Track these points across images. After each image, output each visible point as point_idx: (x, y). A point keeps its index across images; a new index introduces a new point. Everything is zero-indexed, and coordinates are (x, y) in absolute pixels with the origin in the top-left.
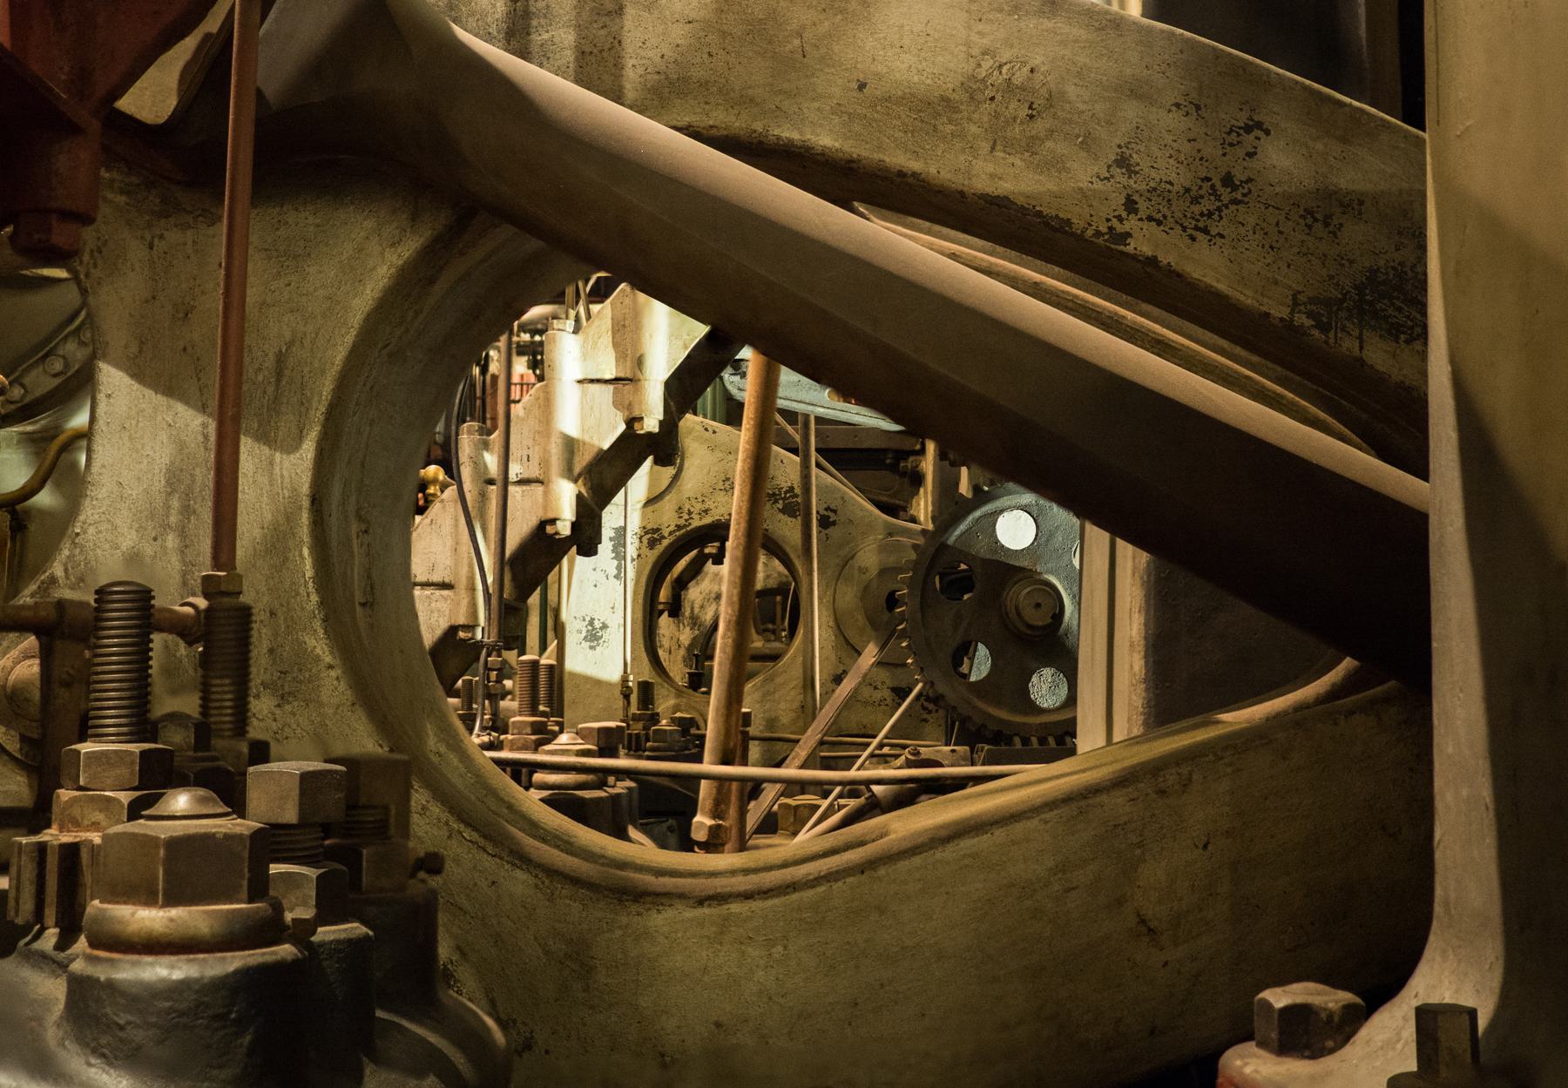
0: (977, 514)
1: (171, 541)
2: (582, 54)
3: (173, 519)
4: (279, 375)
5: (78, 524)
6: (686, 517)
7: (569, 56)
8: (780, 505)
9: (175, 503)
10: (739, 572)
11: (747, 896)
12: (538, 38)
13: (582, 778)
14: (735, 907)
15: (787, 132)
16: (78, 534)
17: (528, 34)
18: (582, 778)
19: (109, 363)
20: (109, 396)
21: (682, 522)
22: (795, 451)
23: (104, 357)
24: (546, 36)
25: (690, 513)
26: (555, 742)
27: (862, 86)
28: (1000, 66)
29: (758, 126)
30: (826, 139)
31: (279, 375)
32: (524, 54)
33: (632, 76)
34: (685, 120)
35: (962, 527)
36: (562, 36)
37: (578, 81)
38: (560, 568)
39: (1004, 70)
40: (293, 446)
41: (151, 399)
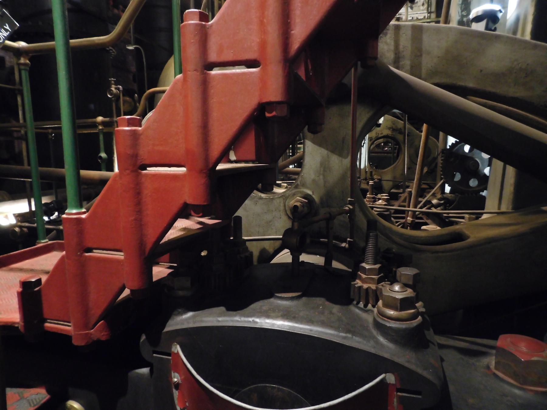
0: (460, 145)
1: (321, 177)
2: (412, 67)
3: (322, 172)
4: (343, 142)
5: (303, 173)
6: (378, 135)
7: (408, 67)
8: (398, 132)
9: (322, 169)
10: (420, 168)
11: (443, 252)
12: (401, 63)
13: (384, 210)
14: (440, 254)
15: (462, 83)
16: (303, 176)
17: (399, 62)
18: (384, 210)
19: (308, 140)
20: (308, 147)
21: (377, 136)
22: (402, 120)
23: (307, 139)
24: (403, 63)
25: (378, 134)
26: (378, 202)
27: (481, 71)
28: (519, 63)
29: (454, 82)
30: (471, 84)
31: (343, 142)
32: (397, 68)
33: (424, 72)
34: (437, 81)
35: (457, 148)
36: (407, 63)
37: (412, 74)
38: (428, 199)
39: (520, 65)
40: (347, 157)
41: (316, 147)
